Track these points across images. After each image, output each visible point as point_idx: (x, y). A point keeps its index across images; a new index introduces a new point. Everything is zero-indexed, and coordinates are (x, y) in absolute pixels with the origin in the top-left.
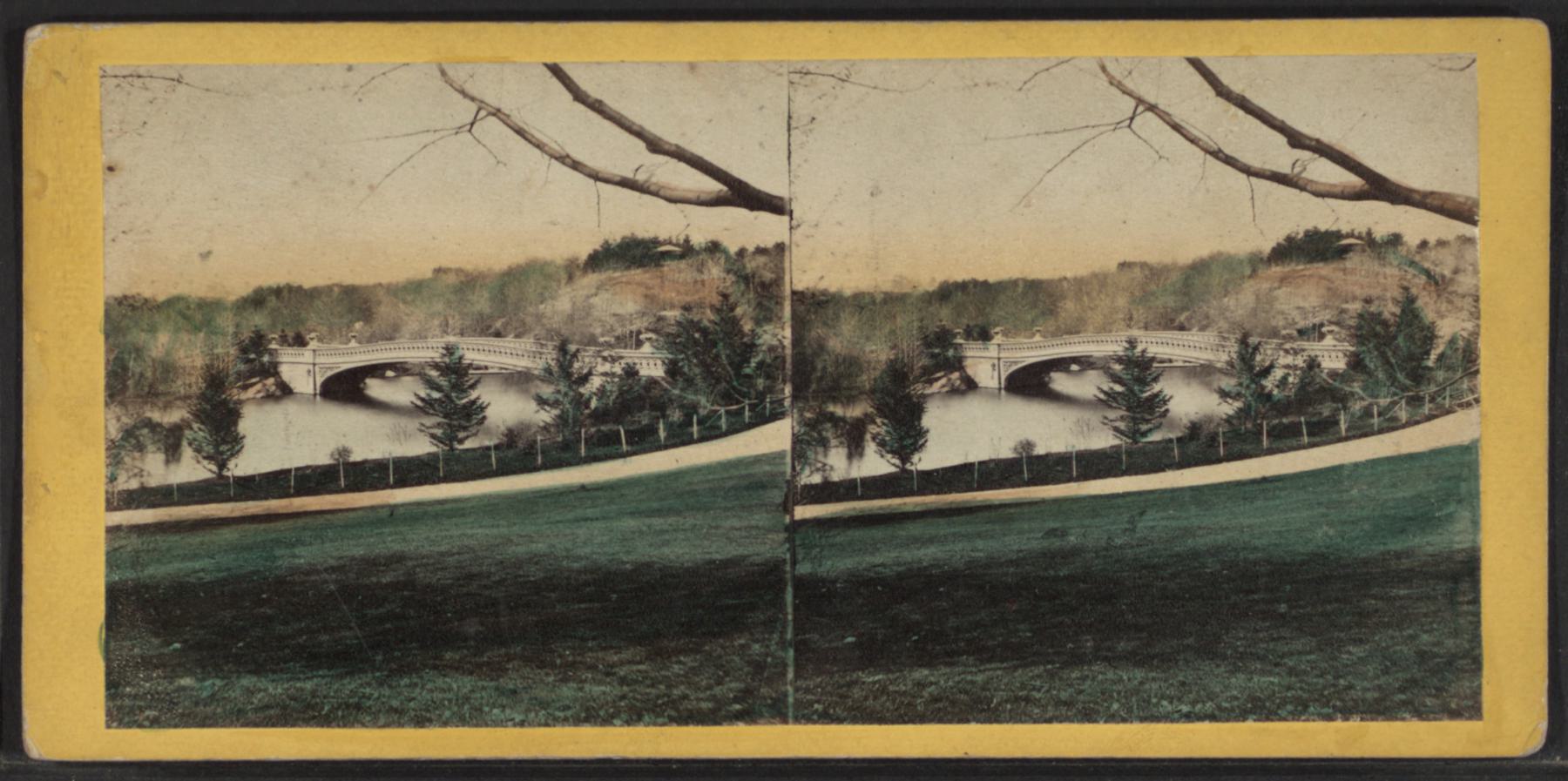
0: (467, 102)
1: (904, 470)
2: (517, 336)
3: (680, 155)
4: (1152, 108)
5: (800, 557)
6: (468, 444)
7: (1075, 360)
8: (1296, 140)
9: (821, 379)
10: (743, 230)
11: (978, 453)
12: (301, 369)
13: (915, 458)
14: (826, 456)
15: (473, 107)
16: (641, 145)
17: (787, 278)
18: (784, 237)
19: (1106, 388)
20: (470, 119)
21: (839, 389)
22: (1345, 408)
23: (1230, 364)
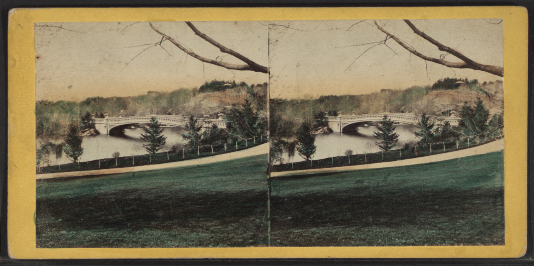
0: (159, 35)
1: (308, 160)
2: (176, 115)
3: (232, 53)
4: (392, 37)
5: (272, 190)
6: (159, 151)
7: (366, 123)
8: (441, 48)
10: (253, 78)
11: (333, 154)
12: (102, 126)
13: (312, 156)
15: (161, 36)
17: (268, 95)
18: (267, 81)
21: (286, 133)
22: (458, 139)
23: (419, 124)
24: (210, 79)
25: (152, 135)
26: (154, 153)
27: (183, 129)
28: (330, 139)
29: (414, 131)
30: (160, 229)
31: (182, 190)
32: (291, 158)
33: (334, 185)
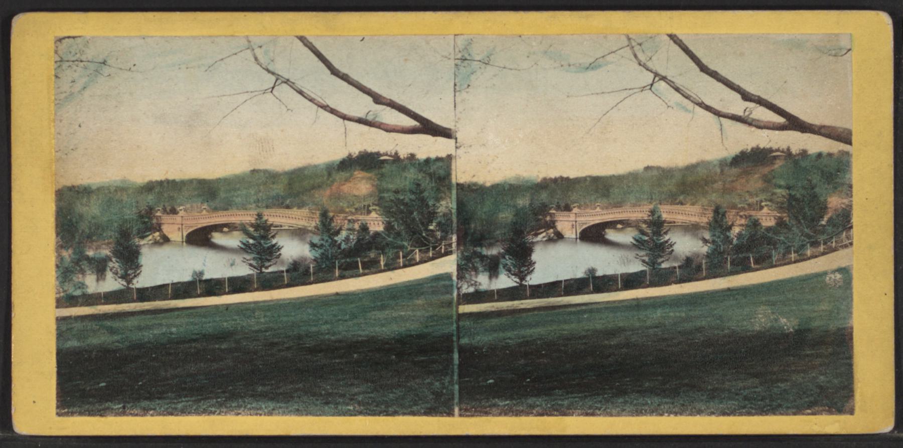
1: (521, 285)
2: (634, 205)
3: (393, 105)
5: (461, 335)
6: (270, 270)
7: (620, 222)
8: (746, 96)
10: (427, 147)
12: (174, 229)
13: (528, 278)
15: (273, 78)
16: (370, 99)
17: (453, 173)
18: (452, 151)
21: (480, 239)
22: (383, 253)
24: (355, 150)
26: (261, 272)
28: (560, 249)
30: (659, 395)
33: (566, 327)
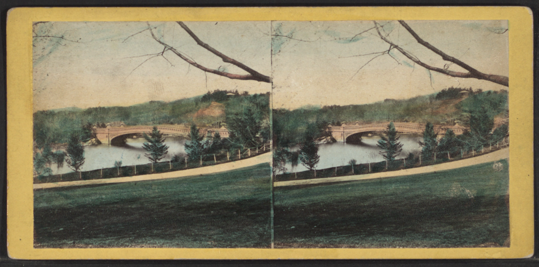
0: (161, 45)
1: (311, 170)
2: (379, 122)
3: (234, 63)
4: (396, 47)
5: (275, 200)
6: (161, 161)
8: (445, 57)
9: (283, 139)
10: (255, 88)
11: (337, 163)
12: (104, 136)
14: (284, 165)
15: (163, 47)
16: (221, 59)
17: (271, 103)
18: (270, 90)
19: (146, 144)
20: (388, 49)
21: (287, 143)
22: (229, 151)
23: (188, 135)
25: (389, 142)
26: (156, 162)
27: (186, 138)
28: (334, 149)
29: (418, 140)
31: (417, 196)
32: (295, 167)
33: (338, 195)
